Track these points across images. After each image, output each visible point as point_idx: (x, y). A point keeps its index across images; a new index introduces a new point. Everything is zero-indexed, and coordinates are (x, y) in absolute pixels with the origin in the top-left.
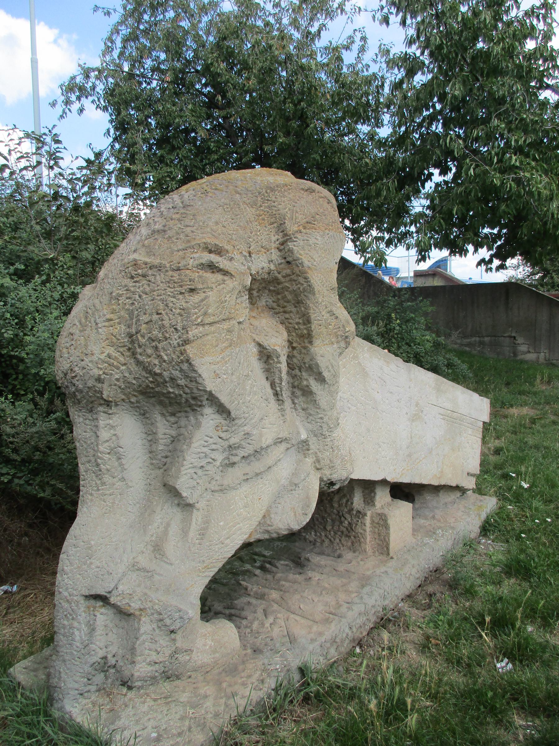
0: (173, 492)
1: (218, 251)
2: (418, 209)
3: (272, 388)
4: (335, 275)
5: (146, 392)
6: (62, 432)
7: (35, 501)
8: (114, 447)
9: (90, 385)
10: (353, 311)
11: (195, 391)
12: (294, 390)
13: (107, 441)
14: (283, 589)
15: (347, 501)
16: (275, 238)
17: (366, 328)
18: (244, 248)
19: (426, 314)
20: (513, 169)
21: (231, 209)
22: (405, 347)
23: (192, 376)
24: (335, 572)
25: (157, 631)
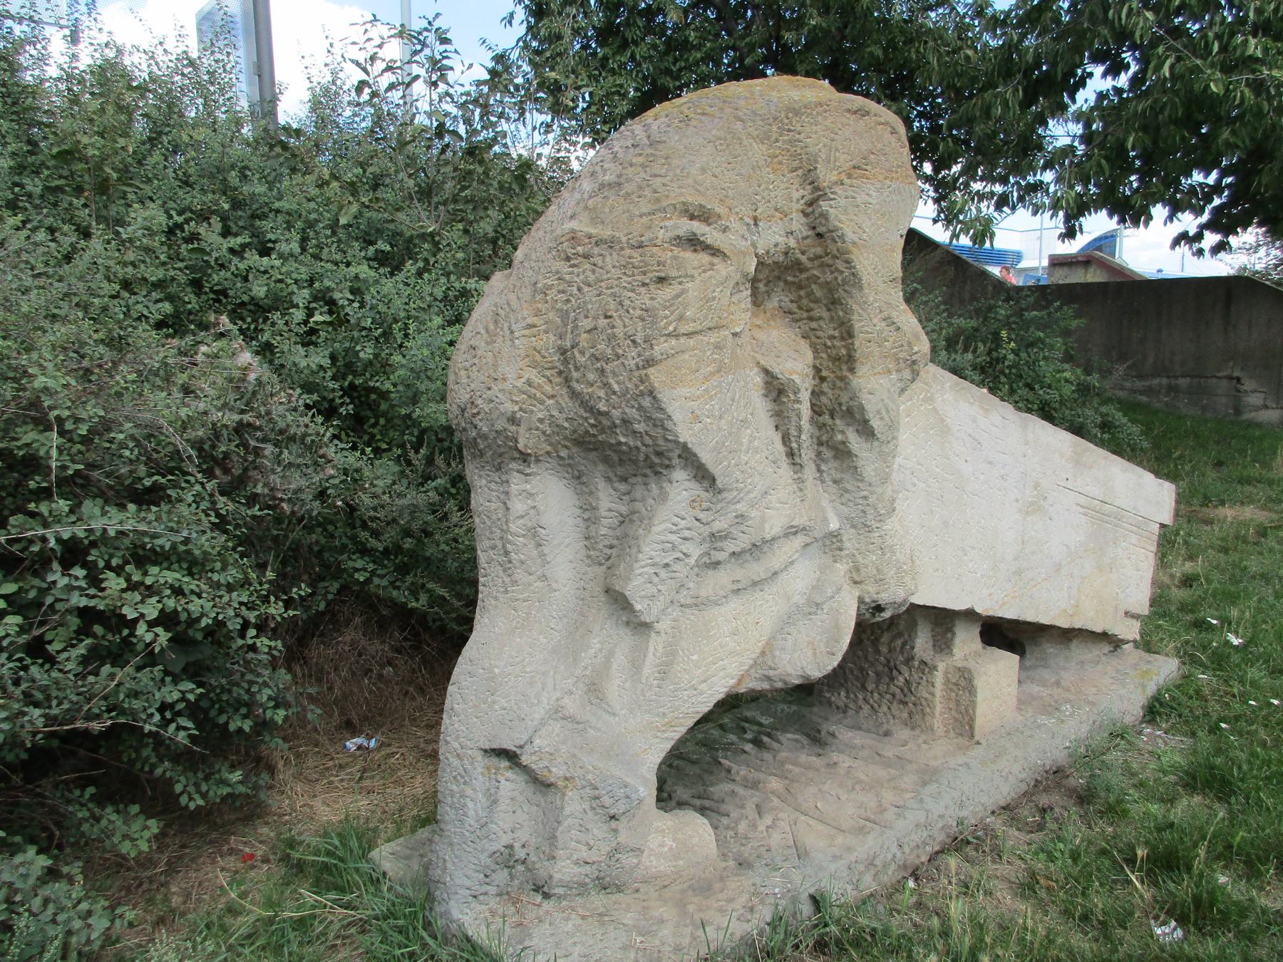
0: (619, 602)
1: (704, 216)
2: (1064, 141)
3: (784, 444)
4: (898, 257)
5: (583, 442)
6: (445, 510)
7: (403, 614)
8: (532, 526)
10: (931, 325)
11: (661, 442)
12: (821, 449)
14: (790, 776)
15: (904, 644)
16: (799, 193)
17: (953, 356)
18: (746, 212)
19: (1066, 333)
20: (1249, 63)
21: (728, 145)
22: (1023, 392)
23: (657, 417)
24: (877, 758)
25: (590, 814)
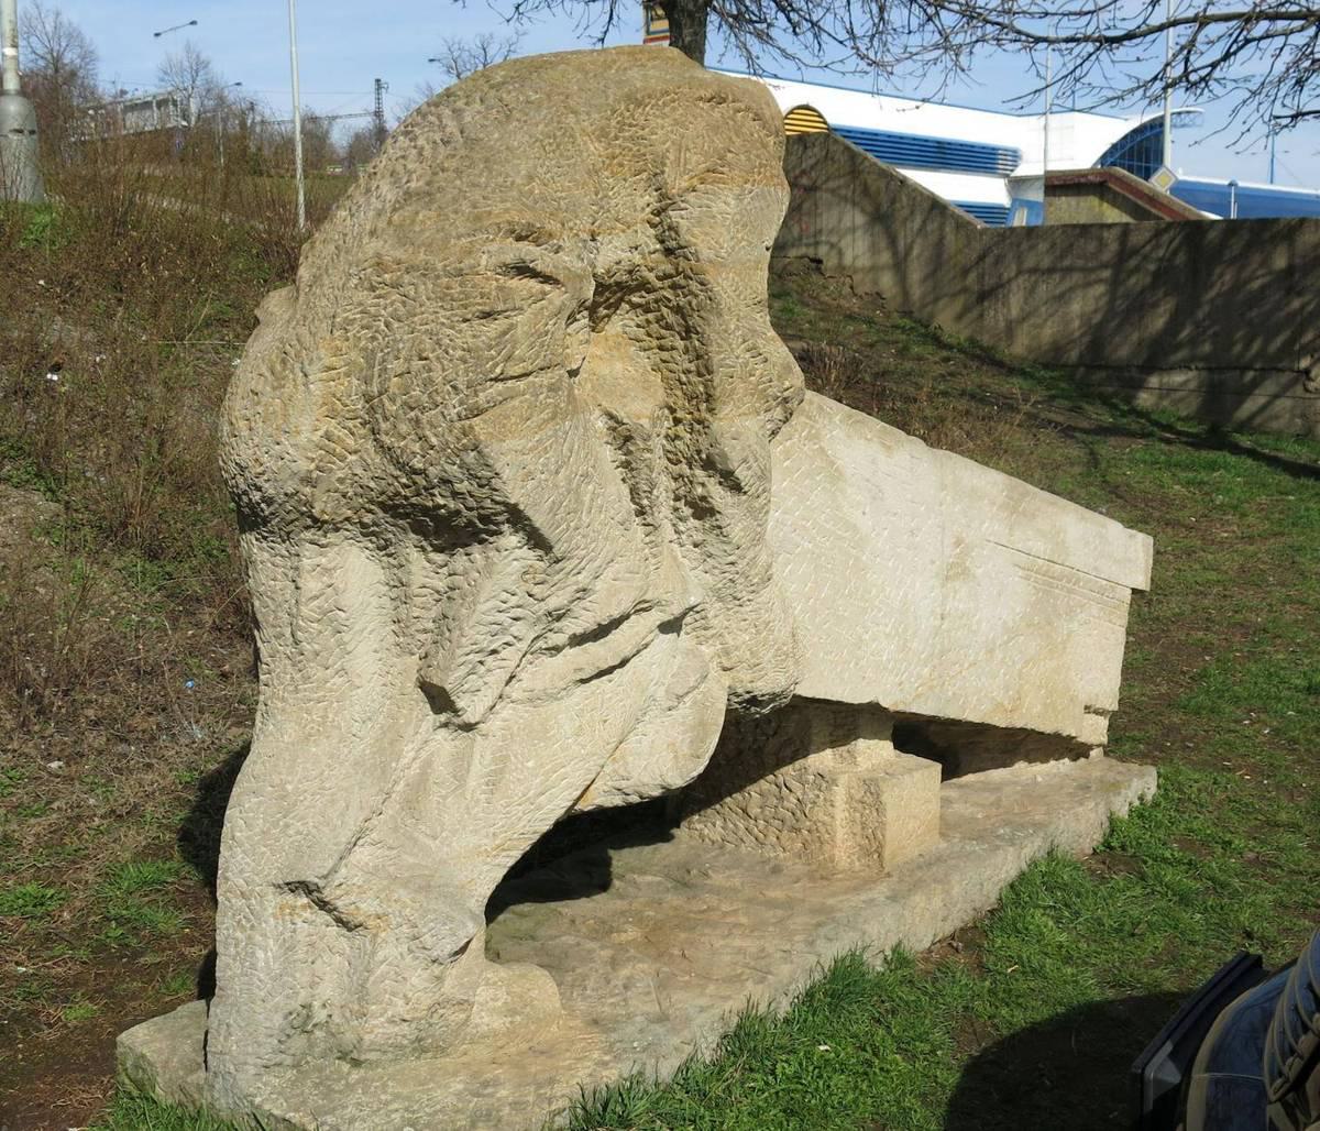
5: (392, 508)
8: (338, 602)
9: (290, 490)
12: (678, 504)
13: (316, 597)
21: (558, 146)
23: (486, 481)
25: (408, 958)
